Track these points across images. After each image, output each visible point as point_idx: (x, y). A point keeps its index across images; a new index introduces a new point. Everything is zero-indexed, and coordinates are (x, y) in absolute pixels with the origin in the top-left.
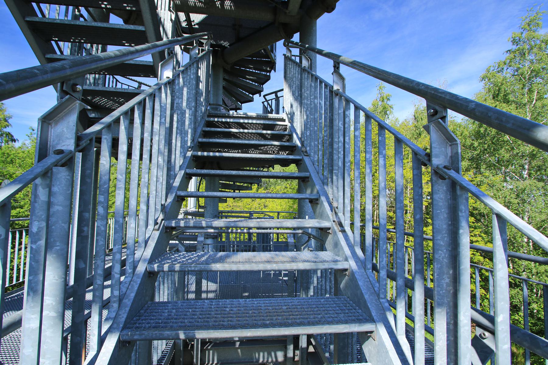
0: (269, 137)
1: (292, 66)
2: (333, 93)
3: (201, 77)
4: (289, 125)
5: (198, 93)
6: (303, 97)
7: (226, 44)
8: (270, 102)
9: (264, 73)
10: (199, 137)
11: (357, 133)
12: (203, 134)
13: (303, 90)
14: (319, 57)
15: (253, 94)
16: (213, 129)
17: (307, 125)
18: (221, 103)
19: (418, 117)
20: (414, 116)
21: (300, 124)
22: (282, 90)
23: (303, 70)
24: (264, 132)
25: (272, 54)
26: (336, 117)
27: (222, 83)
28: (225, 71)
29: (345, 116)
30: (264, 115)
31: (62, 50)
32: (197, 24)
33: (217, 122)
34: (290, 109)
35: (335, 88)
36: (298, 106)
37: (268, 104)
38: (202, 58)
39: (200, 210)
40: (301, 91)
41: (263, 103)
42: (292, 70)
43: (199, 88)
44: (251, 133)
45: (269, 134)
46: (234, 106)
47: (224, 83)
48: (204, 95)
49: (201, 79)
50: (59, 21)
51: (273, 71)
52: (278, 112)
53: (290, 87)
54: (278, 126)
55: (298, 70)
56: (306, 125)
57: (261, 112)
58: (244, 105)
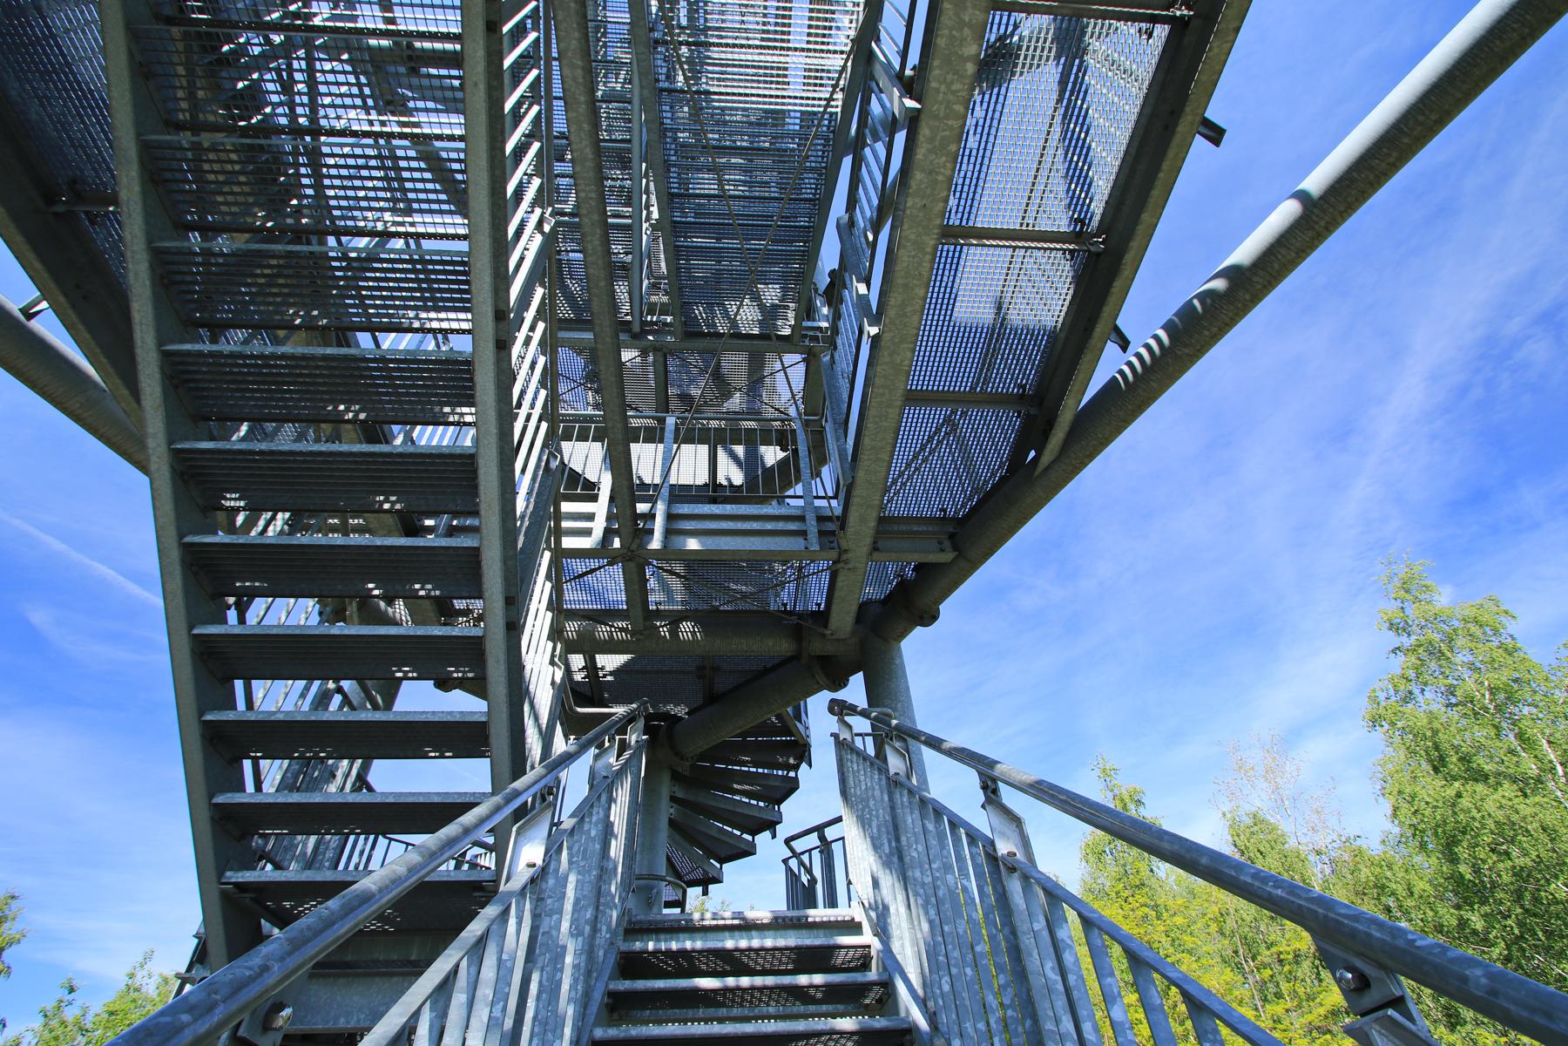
0: (819, 995)
1: (861, 767)
2: (997, 867)
3: (616, 824)
4: (876, 944)
5: (604, 872)
6: (907, 859)
7: (681, 711)
8: (805, 858)
9: (780, 773)
10: (597, 1023)
11: (1117, 1013)
12: (607, 1005)
13: (903, 839)
14: (928, 754)
15: (754, 833)
16: (641, 984)
17: (937, 955)
18: (662, 870)
19: (1247, 848)
20: (1236, 846)
21: (912, 946)
22: (839, 820)
23: (894, 783)
24: (803, 980)
25: (798, 724)
26: (1027, 941)
27: (666, 811)
28: (677, 777)
29: (1057, 948)
30: (795, 913)
31: (262, 778)
32: (611, 673)
33: (656, 952)
34: (871, 890)
35: (1003, 848)
36: (897, 885)
37: (801, 863)
38: (620, 773)
40: (898, 840)
41: (785, 861)
42: (862, 778)
43: (608, 857)
44: (761, 989)
45: (817, 987)
46: (698, 874)
47: (672, 811)
48: (620, 870)
49: (616, 829)
50: (280, 717)
51: (804, 766)
52: (832, 902)
53: (864, 822)
54: (843, 952)
55: (880, 779)
56: (932, 953)
57: (781, 905)
58: (729, 869)
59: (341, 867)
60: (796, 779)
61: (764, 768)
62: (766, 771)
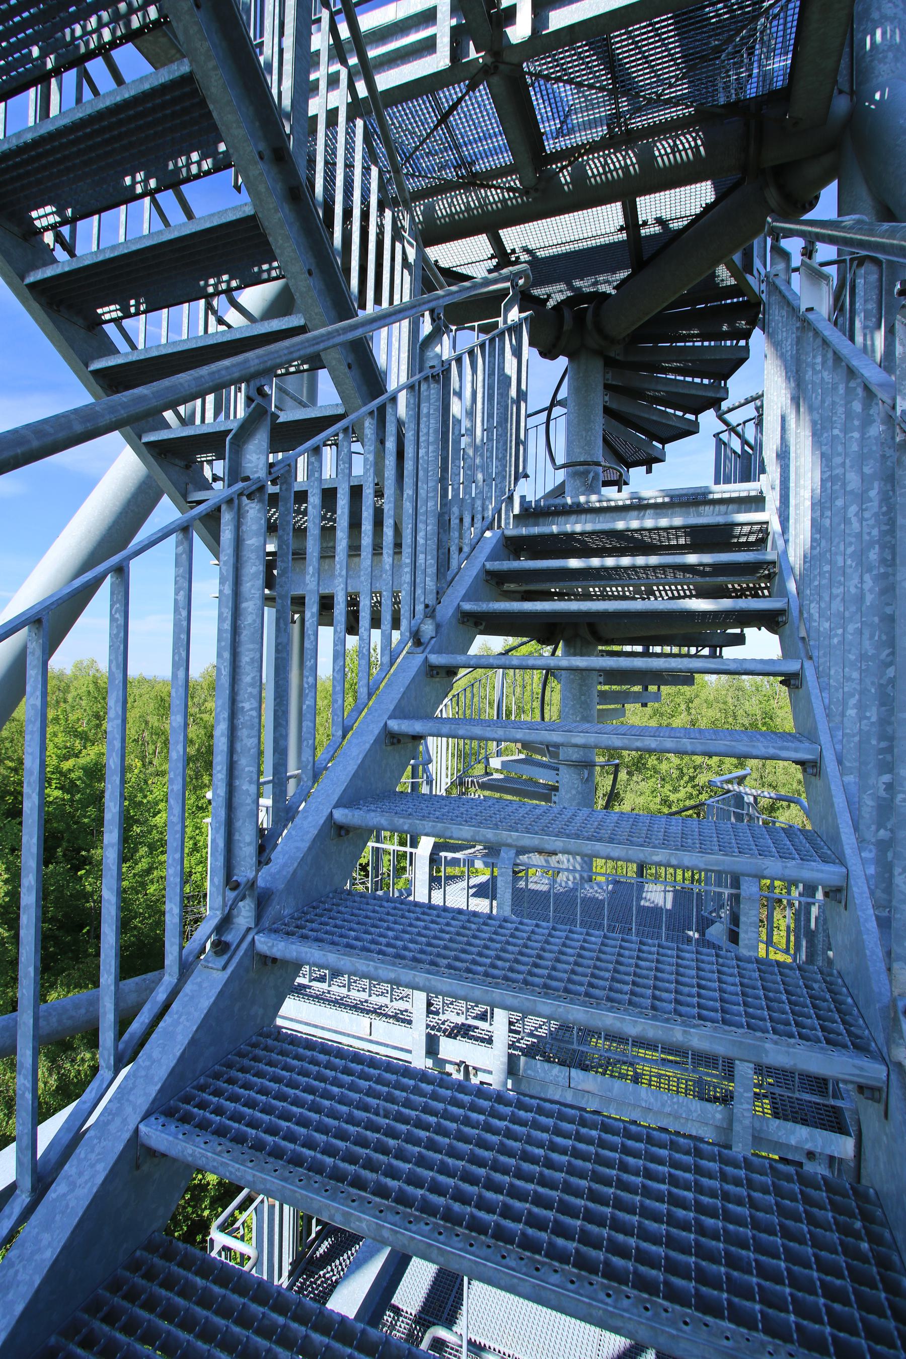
4: (775, 526)
15: (697, 413)
39: (738, 631)
41: (716, 435)
46: (642, 456)
51: (757, 333)
59: (232, 417)
60: (747, 348)
61: (710, 341)
62: (713, 343)
